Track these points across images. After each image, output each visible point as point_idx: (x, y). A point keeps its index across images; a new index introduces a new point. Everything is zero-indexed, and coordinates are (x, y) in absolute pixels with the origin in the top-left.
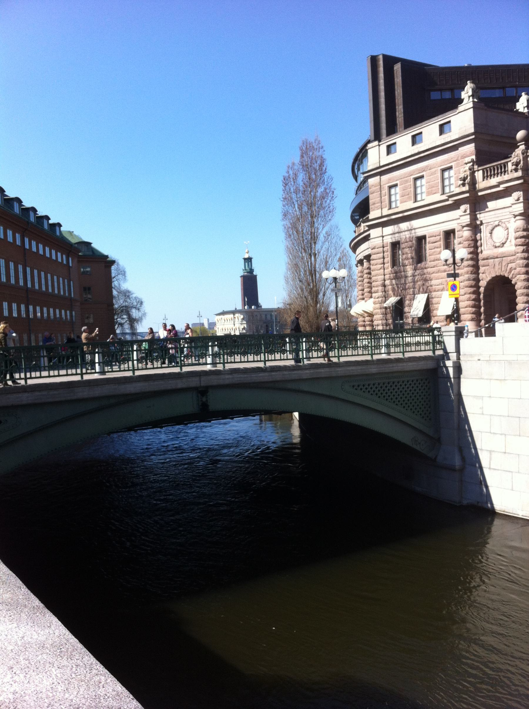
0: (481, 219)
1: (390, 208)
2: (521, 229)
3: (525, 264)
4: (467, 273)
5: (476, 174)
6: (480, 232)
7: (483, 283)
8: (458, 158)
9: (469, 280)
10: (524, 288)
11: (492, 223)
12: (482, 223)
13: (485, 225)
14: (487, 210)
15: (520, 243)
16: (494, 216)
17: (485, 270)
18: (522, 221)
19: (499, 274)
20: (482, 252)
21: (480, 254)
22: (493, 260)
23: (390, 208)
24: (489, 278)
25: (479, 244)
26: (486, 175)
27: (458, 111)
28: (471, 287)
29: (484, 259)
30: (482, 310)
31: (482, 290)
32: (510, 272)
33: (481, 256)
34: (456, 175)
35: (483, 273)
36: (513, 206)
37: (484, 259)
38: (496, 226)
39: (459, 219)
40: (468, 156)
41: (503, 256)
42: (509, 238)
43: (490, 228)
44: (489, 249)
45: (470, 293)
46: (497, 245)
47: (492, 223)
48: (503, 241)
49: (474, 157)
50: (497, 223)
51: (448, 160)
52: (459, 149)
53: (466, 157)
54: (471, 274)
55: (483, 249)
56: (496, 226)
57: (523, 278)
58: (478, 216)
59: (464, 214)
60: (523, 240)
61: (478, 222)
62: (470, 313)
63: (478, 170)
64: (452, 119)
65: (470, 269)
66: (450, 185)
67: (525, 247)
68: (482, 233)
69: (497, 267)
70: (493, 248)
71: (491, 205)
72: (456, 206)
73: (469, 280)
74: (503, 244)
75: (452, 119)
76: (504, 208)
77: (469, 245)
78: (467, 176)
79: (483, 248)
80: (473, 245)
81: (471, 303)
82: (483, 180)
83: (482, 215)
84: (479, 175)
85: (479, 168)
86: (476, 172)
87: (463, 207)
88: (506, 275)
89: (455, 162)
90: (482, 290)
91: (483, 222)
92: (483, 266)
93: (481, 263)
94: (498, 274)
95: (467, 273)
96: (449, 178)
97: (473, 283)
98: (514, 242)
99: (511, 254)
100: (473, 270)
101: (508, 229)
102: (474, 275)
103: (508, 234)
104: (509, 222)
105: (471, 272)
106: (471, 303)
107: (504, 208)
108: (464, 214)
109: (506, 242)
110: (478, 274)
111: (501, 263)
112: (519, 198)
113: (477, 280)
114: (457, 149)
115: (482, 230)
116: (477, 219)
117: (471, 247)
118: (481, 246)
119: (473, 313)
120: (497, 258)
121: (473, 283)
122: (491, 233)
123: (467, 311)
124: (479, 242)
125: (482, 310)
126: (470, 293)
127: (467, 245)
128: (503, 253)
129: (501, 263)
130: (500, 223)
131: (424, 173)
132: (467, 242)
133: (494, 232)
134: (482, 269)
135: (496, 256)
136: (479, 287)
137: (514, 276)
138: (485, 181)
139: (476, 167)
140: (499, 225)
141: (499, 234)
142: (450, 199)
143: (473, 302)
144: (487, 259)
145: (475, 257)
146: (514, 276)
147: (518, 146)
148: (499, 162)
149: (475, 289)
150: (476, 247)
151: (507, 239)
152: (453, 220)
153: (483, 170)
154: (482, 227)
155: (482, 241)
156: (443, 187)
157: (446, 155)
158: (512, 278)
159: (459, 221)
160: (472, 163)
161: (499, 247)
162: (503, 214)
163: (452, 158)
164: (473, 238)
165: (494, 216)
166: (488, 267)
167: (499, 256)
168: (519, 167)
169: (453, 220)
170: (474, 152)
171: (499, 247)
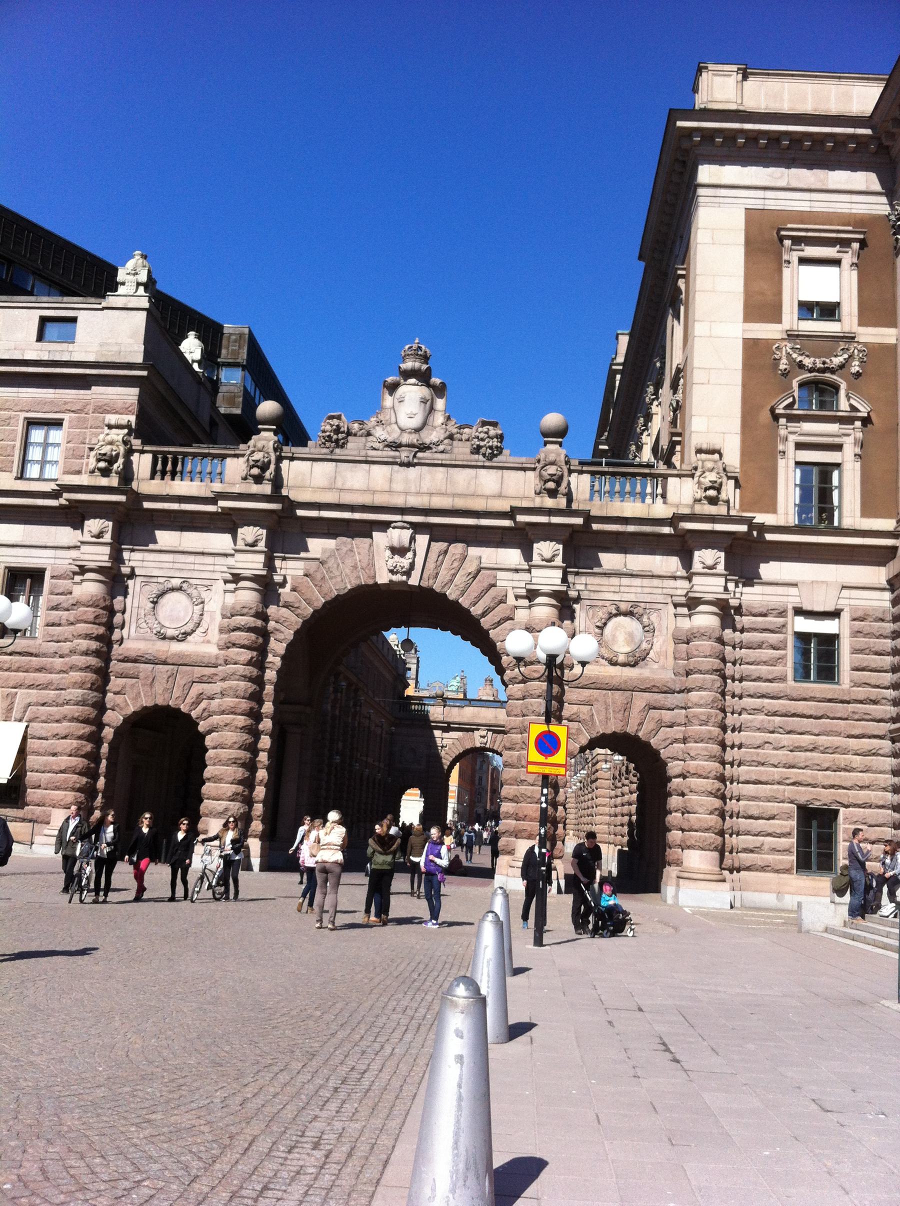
0: (132, 564)
1: (21, 477)
2: (253, 611)
3: (250, 691)
4: (81, 685)
5: (135, 458)
6: (125, 594)
7: (114, 718)
8: (85, 407)
9: (83, 703)
10: (240, 748)
11: (161, 580)
12: (132, 575)
13: (139, 579)
14: (151, 547)
15: (246, 642)
16: (171, 565)
17: (124, 687)
18: (254, 594)
19: (165, 704)
20: (121, 641)
21: (115, 646)
22: (152, 666)
23: (21, 477)
24: (131, 709)
25: (118, 619)
26: (159, 467)
27: (104, 304)
28: (86, 721)
29: (126, 660)
30: (101, 783)
31: (108, 733)
32: (197, 703)
33: (116, 650)
34: (70, 445)
35: (116, 693)
36: (84, 548)
37: (126, 660)
38: (173, 590)
39: (233, 555)
40: (116, 413)
41: (181, 662)
42: (204, 625)
43: (154, 589)
44: (145, 639)
45: (80, 738)
46: (170, 633)
47: (161, 580)
48: (188, 628)
49: (133, 419)
50: (176, 582)
51: (52, 402)
52: (94, 389)
53: (109, 412)
54: (90, 689)
55: (125, 636)
56: (173, 590)
57: (241, 724)
58: (126, 555)
59: (94, 540)
60: (253, 636)
61: (125, 570)
62: (73, 789)
63: (142, 452)
64: (82, 316)
65: (90, 676)
66: (43, 463)
67: (255, 653)
68: (129, 597)
69: (159, 688)
70: (155, 638)
71: (165, 538)
72: (73, 515)
73: (83, 703)
74: (186, 634)
75: (83, 317)
76: (203, 554)
77: (96, 617)
78: (118, 455)
79: (125, 632)
80: (104, 620)
81: (79, 762)
82: (152, 478)
83: (137, 556)
84: (142, 463)
85: (146, 448)
86: (136, 455)
87: (93, 525)
88: (184, 708)
89: (73, 415)
90: (108, 733)
91: (137, 572)
92: (121, 676)
93: (115, 666)
94: (160, 701)
95: (81, 685)
96: (46, 445)
97: (91, 712)
98: (215, 635)
99: (206, 661)
100: (97, 680)
101: (203, 602)
102: (95, 694)
103: (202, 615)
104: (208, 588)
105: (92, 684)
106: (79, 762)
107: (203, 554)
108: (94, 540)
109: (193, 631)
110: (104, 693)
111: (172, 676)
112: (256, 541)
113: (101, 707)
114: (88, 387)
115: (130, 590)
116: (122, 561)
117: (99, 624)
118: (122, 627)
119: (79, 790)
120: (165, 663)
121: (91, 712)
122: (155, 603)
123: (65, 780)
124: (119, 615)
125: (101, 783)
126: (80, 738)
127: (91, 617)
128: (181, 655)
129: (172, 676)
130: (185, 586)
131: (66, 417)
132: (93, 609)
133: (164, 601)
134: (115, 683)
135: (163, 658)
136: (101, 726)
137: (206, 714)
138: (157, 481)
139: (136, 443)
140: (180, 589)
141: (176, 610)
142: (65, 495)
143: (86, 761)
144: (135, 661)
145: (105, 649)
146: (206, 714)
147: (258, 432)
148: (166, 449)
149: (94, 728)
150: (110, 627)
151: (198, 625)
152: (46, 547)
153: (155, 455)
154: (130, 583)
155: (127, 615)
156: (24, 462)
157: (51, 391)
158: (200, 717)
159: (74, 554)
160: (126, 431)
161: (172, 638)
162: (197, 567)
163: (65, 403)
164: (108, 603)
165: (171, 565)
166: (134, 680)
167: (169, 661)
168: (115, 466)
169: (46, 547)
170: (135, 408)
171: (172, 638)
